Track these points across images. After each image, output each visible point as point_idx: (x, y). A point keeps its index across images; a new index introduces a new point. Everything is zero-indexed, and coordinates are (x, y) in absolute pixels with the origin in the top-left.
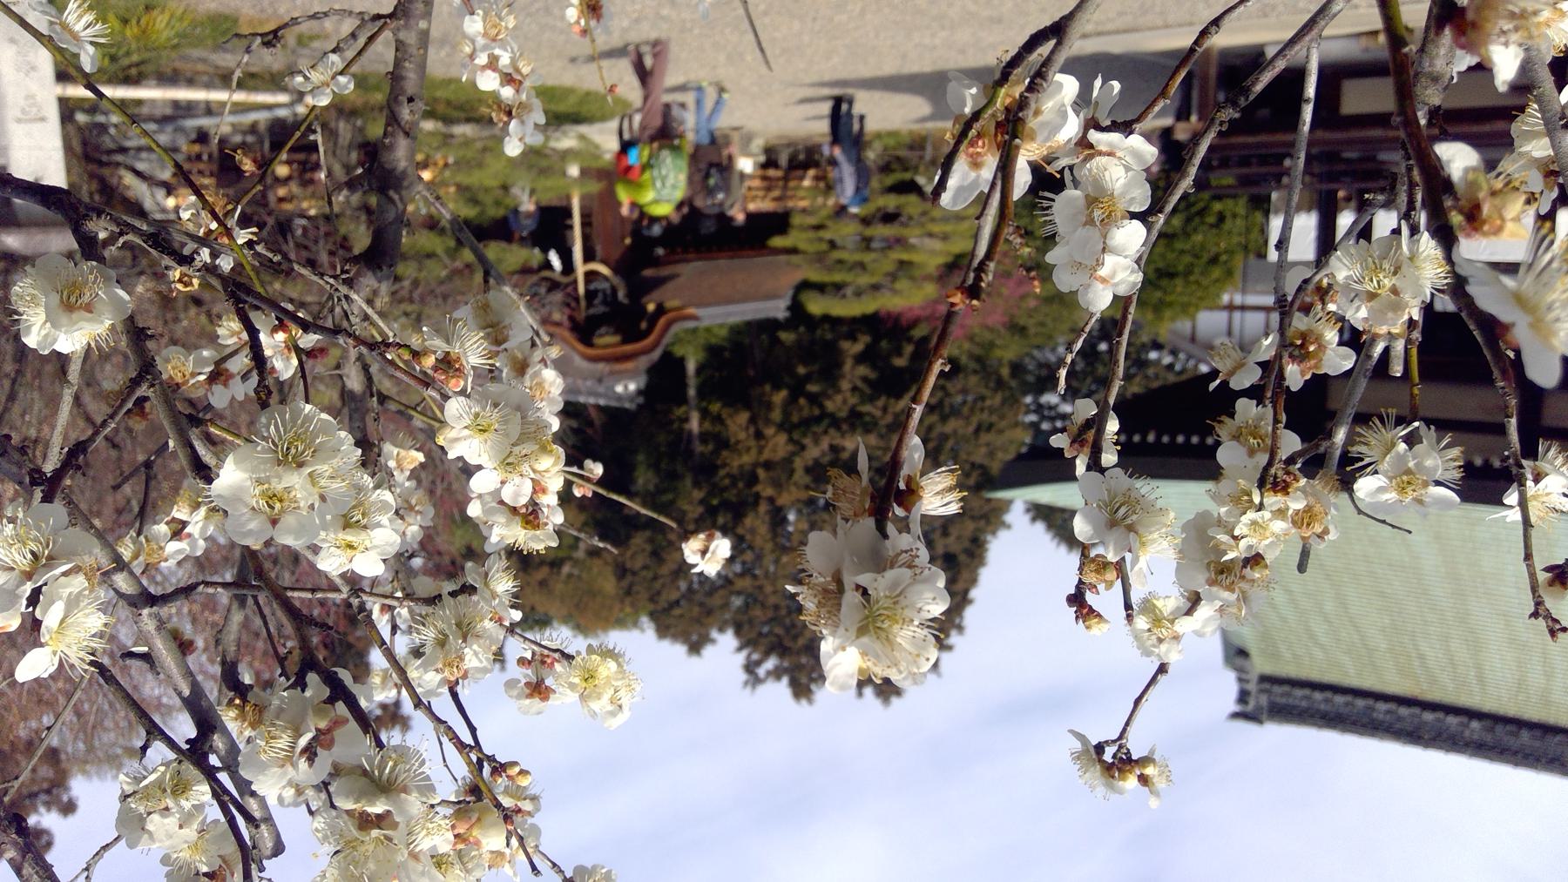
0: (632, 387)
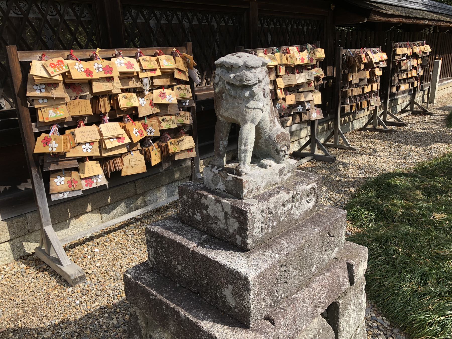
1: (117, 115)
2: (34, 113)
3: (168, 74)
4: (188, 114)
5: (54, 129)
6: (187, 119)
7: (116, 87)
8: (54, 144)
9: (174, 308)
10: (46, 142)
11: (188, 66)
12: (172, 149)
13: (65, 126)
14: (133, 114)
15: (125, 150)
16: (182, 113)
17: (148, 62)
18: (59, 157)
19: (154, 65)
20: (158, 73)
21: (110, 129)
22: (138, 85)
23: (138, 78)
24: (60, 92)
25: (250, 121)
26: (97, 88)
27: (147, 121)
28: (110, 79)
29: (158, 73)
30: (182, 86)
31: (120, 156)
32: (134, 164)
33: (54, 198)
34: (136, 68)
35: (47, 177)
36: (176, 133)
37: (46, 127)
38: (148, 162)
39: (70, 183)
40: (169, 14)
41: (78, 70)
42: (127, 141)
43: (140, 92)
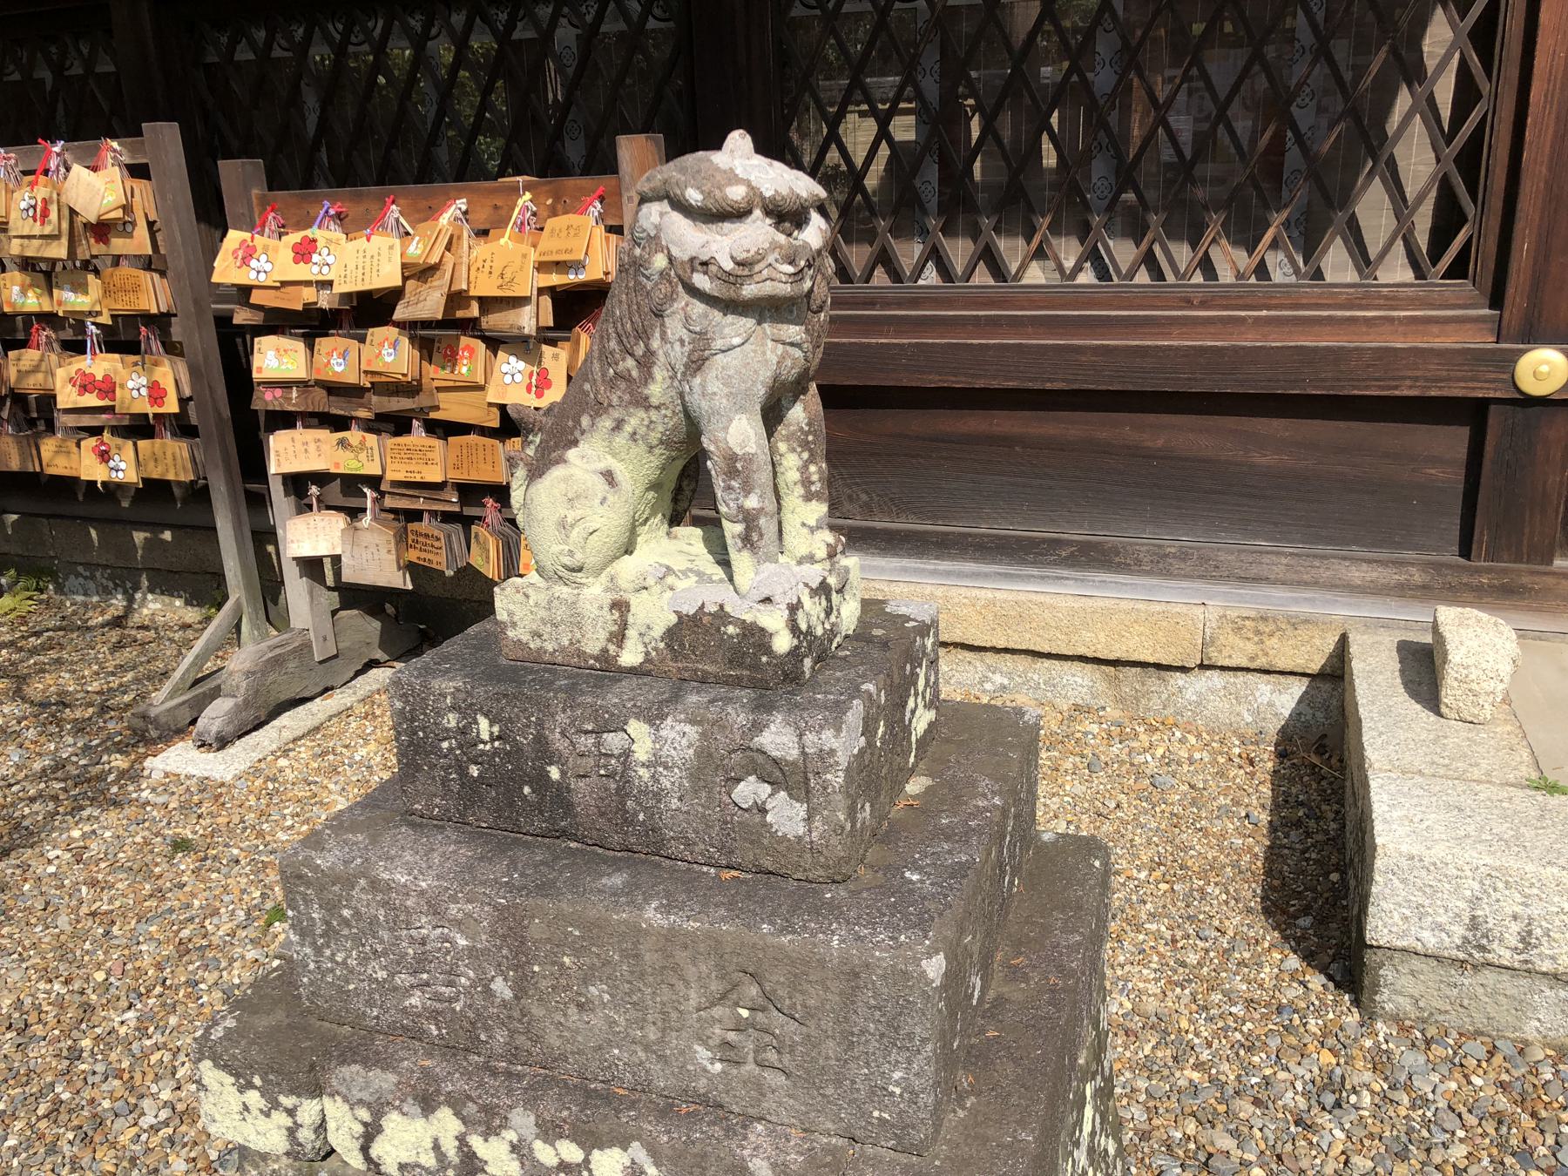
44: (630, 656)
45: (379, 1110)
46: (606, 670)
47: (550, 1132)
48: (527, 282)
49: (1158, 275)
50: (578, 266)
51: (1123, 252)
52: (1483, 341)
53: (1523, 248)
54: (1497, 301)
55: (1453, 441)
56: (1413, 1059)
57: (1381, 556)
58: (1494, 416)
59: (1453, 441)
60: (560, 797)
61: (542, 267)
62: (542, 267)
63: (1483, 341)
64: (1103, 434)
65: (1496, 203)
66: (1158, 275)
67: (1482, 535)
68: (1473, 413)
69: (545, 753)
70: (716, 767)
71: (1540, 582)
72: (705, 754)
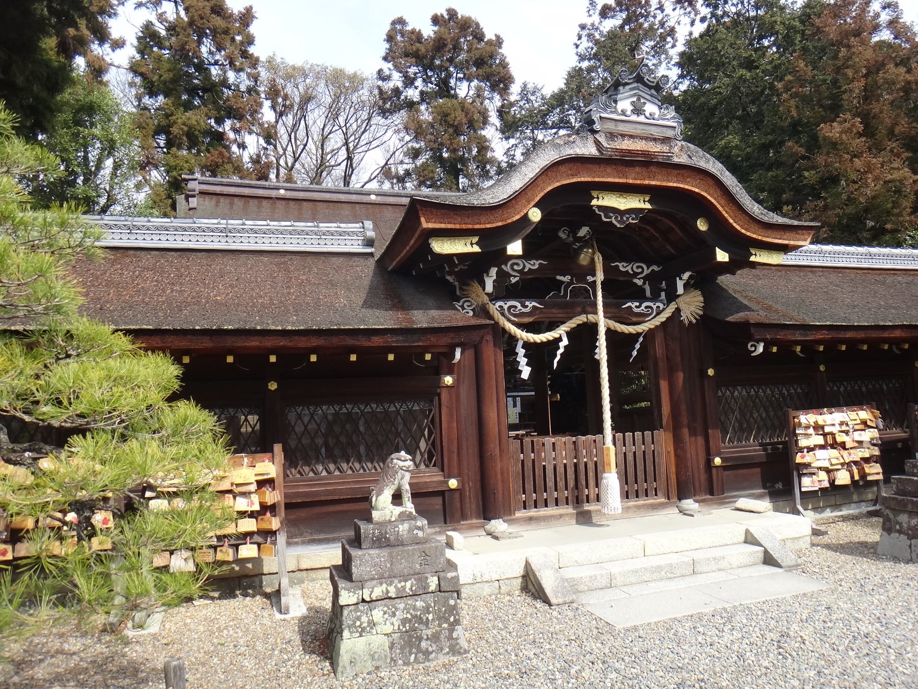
0: (625, 104)
1: (835, 445)
2: (797, 441)
3: (864, 423)
4: (876, 448)
5: (805, 450)
6: (876, 452)
7: (835, 430)
8: (808, 458)
9: (527, 364)
10: (803, 457)
11: (875, 417)
12: (867, 471)
13: (810, 449)
14: (843, 446)
15: (840, 467)
16: (872, 447)
17: (853, 415)
18: (808, 465)
19: (856, 417)
20: (859, 422)
21: (833, 453)
22: (847, 428)
23: (847, 425)
24: (811, 431)
25: (514, 484)
26: (827, 429)
27: (851, 451)
28: (833, 425)
29: (859, 422)
30: (872, 430)
31: (838, 470)
32: (843, 478)
33: (803, 489)
34: (848, 419)
35: (800, 476)
36: (866, 460)
37: (801, 450)
38: (852, 477)
39: (813, 482)
40: (873, 382)
41: (820, 419)
42: (842, 461)
43: (847, 433)
44: (393, 519)
45: (373, 588)
46: (390, 521)
47: (400, 582)
48: (253, 479)
49: (365, 470)
50: (267, 474)
51: (344, 466)
52: (442, 479)
53: (446, 460)
54: (443, 471)
55: (438, 501)
56: (470, 603)
57: (458, 505)
58: (446, 494)
59: (438, 501)
60: (388, 539)
61: (256, 475)
62: (256, 475)
63: (442, 479)
64: (362, 507)
65: (439, 452)
66: (365, 470)
67: (448, 519)
68: (442, 493)
69: (386, 533)
70: (410, 530)
71: (459, 527)
72: (410, 528)
